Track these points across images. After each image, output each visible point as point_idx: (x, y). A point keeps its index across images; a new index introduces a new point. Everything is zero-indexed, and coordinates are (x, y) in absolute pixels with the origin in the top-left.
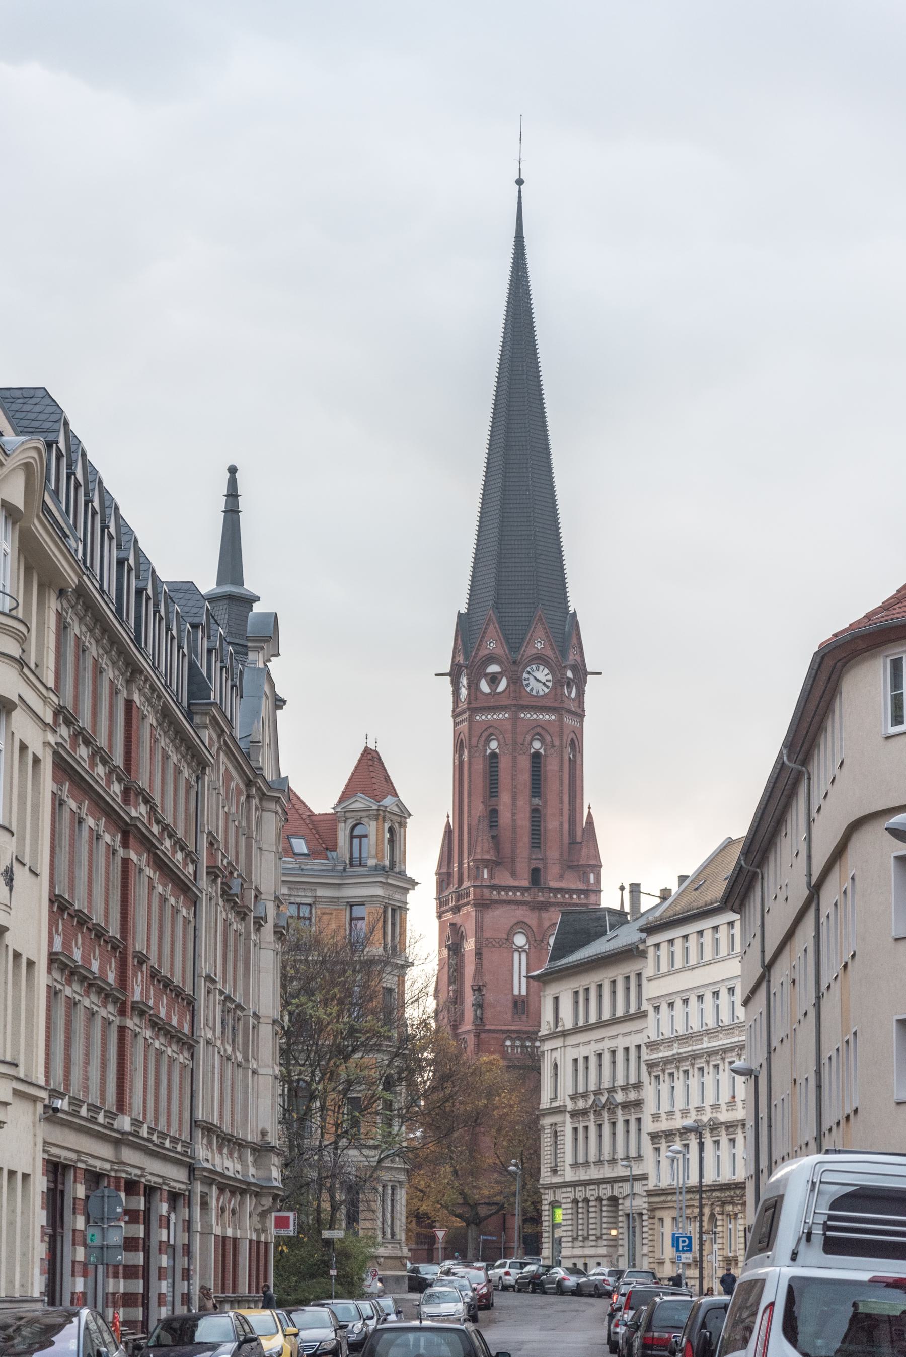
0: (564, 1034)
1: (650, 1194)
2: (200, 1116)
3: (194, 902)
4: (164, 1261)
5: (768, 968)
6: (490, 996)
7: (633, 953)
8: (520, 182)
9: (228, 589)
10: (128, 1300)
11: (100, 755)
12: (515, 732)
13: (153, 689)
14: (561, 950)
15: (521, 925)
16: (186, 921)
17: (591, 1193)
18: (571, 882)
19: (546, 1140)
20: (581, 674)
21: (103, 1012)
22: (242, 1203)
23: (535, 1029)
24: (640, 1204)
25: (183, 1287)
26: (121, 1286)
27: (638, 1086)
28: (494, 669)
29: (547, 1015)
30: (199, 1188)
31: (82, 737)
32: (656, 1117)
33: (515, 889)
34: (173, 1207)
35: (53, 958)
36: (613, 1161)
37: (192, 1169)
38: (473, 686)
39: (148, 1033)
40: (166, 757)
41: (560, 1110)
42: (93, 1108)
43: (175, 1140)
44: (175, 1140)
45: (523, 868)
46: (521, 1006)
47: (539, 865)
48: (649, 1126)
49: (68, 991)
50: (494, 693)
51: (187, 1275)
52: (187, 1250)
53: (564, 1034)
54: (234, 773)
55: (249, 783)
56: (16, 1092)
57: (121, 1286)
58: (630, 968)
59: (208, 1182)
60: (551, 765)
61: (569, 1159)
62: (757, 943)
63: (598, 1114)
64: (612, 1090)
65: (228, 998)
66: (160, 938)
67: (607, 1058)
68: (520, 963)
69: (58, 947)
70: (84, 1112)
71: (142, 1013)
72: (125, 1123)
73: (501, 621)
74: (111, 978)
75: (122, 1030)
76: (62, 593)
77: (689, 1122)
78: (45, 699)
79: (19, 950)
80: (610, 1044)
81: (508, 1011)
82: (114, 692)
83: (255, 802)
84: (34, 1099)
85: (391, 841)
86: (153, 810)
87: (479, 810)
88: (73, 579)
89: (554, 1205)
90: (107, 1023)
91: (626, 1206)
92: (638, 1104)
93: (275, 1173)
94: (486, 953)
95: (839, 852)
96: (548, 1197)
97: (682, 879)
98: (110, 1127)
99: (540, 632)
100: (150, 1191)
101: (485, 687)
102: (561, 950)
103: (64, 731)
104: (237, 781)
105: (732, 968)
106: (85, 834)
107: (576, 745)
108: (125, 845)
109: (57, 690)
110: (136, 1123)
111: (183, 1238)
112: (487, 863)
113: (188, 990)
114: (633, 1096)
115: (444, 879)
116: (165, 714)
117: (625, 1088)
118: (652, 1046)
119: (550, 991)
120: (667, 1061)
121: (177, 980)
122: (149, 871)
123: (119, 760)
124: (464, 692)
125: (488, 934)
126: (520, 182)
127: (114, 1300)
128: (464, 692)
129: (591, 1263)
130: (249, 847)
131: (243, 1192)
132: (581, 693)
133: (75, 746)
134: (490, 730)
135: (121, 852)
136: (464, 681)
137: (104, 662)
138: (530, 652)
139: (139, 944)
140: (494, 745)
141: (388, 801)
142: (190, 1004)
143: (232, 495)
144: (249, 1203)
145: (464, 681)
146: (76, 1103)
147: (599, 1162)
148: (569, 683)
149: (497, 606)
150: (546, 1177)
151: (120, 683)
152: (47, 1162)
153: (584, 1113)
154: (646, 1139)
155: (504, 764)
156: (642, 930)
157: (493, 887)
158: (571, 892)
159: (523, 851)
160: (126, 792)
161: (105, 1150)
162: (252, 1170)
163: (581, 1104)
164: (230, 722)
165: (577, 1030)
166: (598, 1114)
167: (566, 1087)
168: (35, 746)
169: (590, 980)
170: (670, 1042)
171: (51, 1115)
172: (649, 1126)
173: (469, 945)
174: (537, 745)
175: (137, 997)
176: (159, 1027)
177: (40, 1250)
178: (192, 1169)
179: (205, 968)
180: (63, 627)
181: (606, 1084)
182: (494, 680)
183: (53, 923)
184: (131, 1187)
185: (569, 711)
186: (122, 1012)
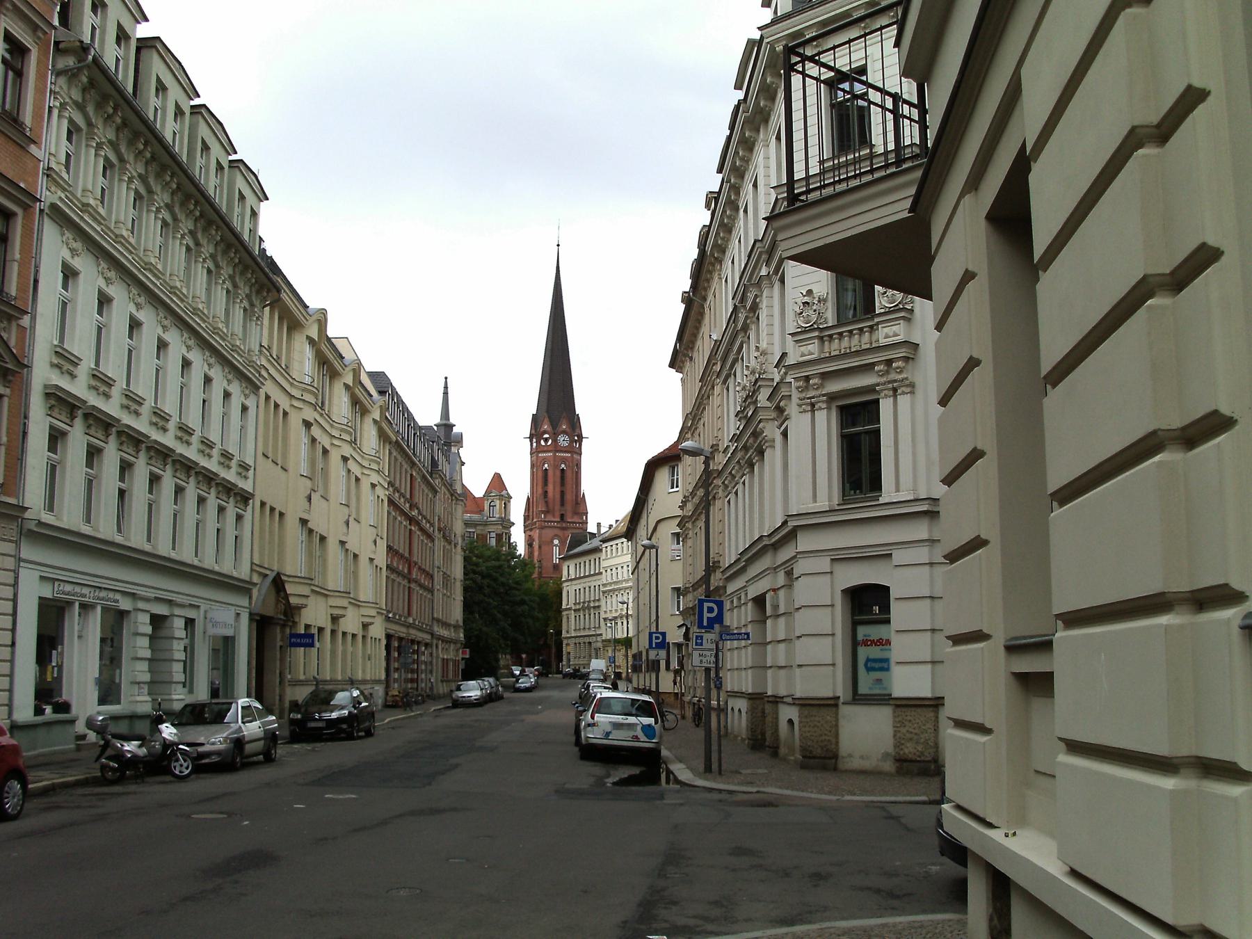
0: (572, 580)
1: (603, 641)
2: (435, 616)
3: (433, 541)
4: (423, 667)
5: (638, 563)
6: (544, 564)
7: (597, 550)
8: (558, 245)
9: (444, 422)
10: (412, 681)
11: (402, 495)
12: (554, 461)
13: (420, 469)
14: (571, 547)
15: (556, 536)
16: (430, 547)
17: (581, 640)
18: (576, 519)
19: (564, 620)
20: (581, 438)
21: (403, 583)
22: (450, 646)
23: (559, 576)
24: (600, 645)
25: (429, 676)
26: (410, 676)
27: (599, 600)
28: (546, 436)
29: (565, 573)
30: (435, 642)
31: (397, 490)
32: (605, 612)
33: (555, 522)
34: (426, 649)
35: (388, 566)
36: (589, 629)
37: (432, 635)
38: (538, 442)
39: (418, 588)
40: (423, 491)
41: (570, 609)
42: (400, 616)
43: (427, 625)
44: (427, 625)
45: (558, 514)
46: (557, 568)
47: (563, 512)
48: (603, 615)
49: (392, 577)
50: (546, 445)
51: (431, 672)
52: (431, 663)
53: (572, 580)
54: (447, 492)
55: (452, 495)
56: (378, 613)
57: (410, 676)
58: (596, 556)
59: (439, 639)
60: (569, 475)
61: (573, 628)
62: (634, 555)
63: (584, 610)
64: (589, 602)
65: (445, 573)
66: (393, 531)
67: (587, 589)
68: (556, 550)
69: (389, 563)
70: (397, 617)
71: (416, 582)
72: (410, 620)
73: (549, 417)
74: (406, 571)
75: (409, 588)
76: (390, 443)
77: (617, 614)
78: (385, 480)
79: (264, 500)
80: (589, 584)
81: (551, 570)
82: (406, 472)
83: (454, 502)
84: (382, 614)
85: (505, 507)
86: (419, 511)
87: (540, 491)
88: (394, 439)
89: (568, 645)
90: (404, 586)
91: (594, 645)
92: (599, 607)
93: (462, 635)
94: (543, 547)
95: (655, 529)
96: (565, 642)
97: (617, 521)
98: (405, 621)
99: (564, 421)
100: (419, 643)
101: (543, 443)
102: (571, 547)
103: (391, 489)
104: (448, 495)
105: (628, 558)
106: (398, 523)
107: (578, 465)
108: (410, 524)
109: (388, 476)
110: (414, 620)
111: (430, 659)
112: (543, 512)
113: (431, 572)
114: (597, 604)
115: (526, 518)
116: (424, 477)
117: (594, 601)
118: (604, 585)
119: (567, 563)
120: (610, 591)
121: (427, 569)
122: (418, 533)
123: (408, 497)
124: (535, 445)
125: (543, 539)
126: (558, 245)
127: (407, 681)
128: (535, 445)
129: (582, 667)
130: (452, 518)
131: (450, 642)
132: (580, 445)
133: (394, 494)
134: (544, 460)
135: (409, 527)
136: (534, 440)
137: (404, 463)
138: (561, 429)
139: (415, 559)
140: (546, 465)
141: (504, 493)
142: (432, 577)
143: (446, 387)
144: (452, 646)
145: (534, 440)
146: (395, 615)
147: (589, 629)
148: (576, 441)
149: (548, 412)
150: (564, 634)
151: (409, 469)
152: (386, 634)
153: (579, 610)
154: (602, 620)
155: (550, 473)
156: (601, 541)
157: (545, 521)
158: (576, 523)
159: (557, 507)
160: (410, 506)
161: (404, 630)
162: (453, 634)
163: (578, 607)
164: (445, 475)
165: (576, 579)
166: (584, 610)
167: (572, 600)
168: (382, 497)
169: (582, 560)
170: (610, 584)
171: (388, 619)
172: (603, 615)
173: (536, 545)
174: (563, 466)
175: (414, 577)
176: (421, 586)
177: (384, 664)
178: (432, 635)
179: (437, 563)
180: (390, 453)
181: (587, 600)
182: (546, 440)
183: (387, 554)
184: (413, 642)
185: (576, 453)
186: (409, 582)
